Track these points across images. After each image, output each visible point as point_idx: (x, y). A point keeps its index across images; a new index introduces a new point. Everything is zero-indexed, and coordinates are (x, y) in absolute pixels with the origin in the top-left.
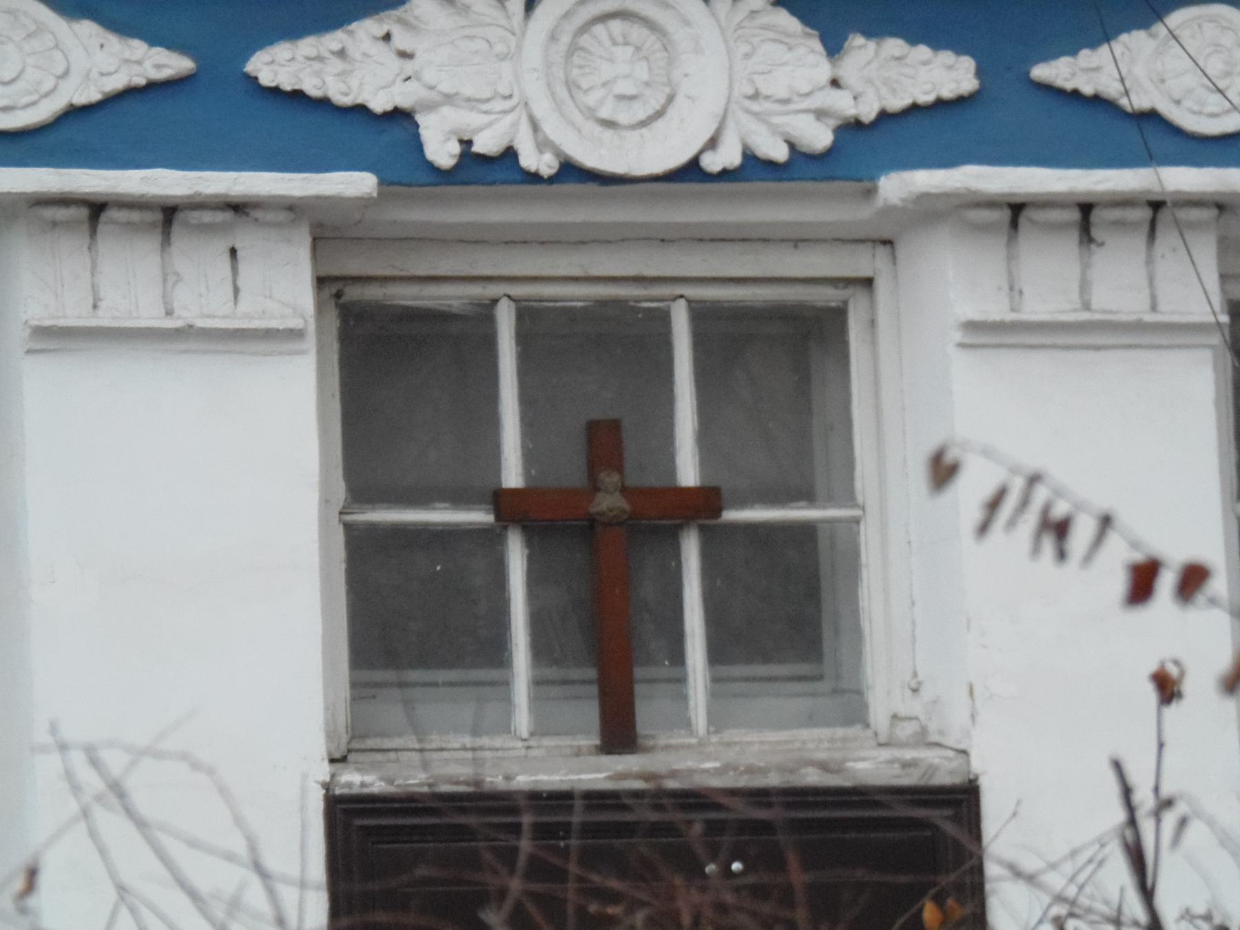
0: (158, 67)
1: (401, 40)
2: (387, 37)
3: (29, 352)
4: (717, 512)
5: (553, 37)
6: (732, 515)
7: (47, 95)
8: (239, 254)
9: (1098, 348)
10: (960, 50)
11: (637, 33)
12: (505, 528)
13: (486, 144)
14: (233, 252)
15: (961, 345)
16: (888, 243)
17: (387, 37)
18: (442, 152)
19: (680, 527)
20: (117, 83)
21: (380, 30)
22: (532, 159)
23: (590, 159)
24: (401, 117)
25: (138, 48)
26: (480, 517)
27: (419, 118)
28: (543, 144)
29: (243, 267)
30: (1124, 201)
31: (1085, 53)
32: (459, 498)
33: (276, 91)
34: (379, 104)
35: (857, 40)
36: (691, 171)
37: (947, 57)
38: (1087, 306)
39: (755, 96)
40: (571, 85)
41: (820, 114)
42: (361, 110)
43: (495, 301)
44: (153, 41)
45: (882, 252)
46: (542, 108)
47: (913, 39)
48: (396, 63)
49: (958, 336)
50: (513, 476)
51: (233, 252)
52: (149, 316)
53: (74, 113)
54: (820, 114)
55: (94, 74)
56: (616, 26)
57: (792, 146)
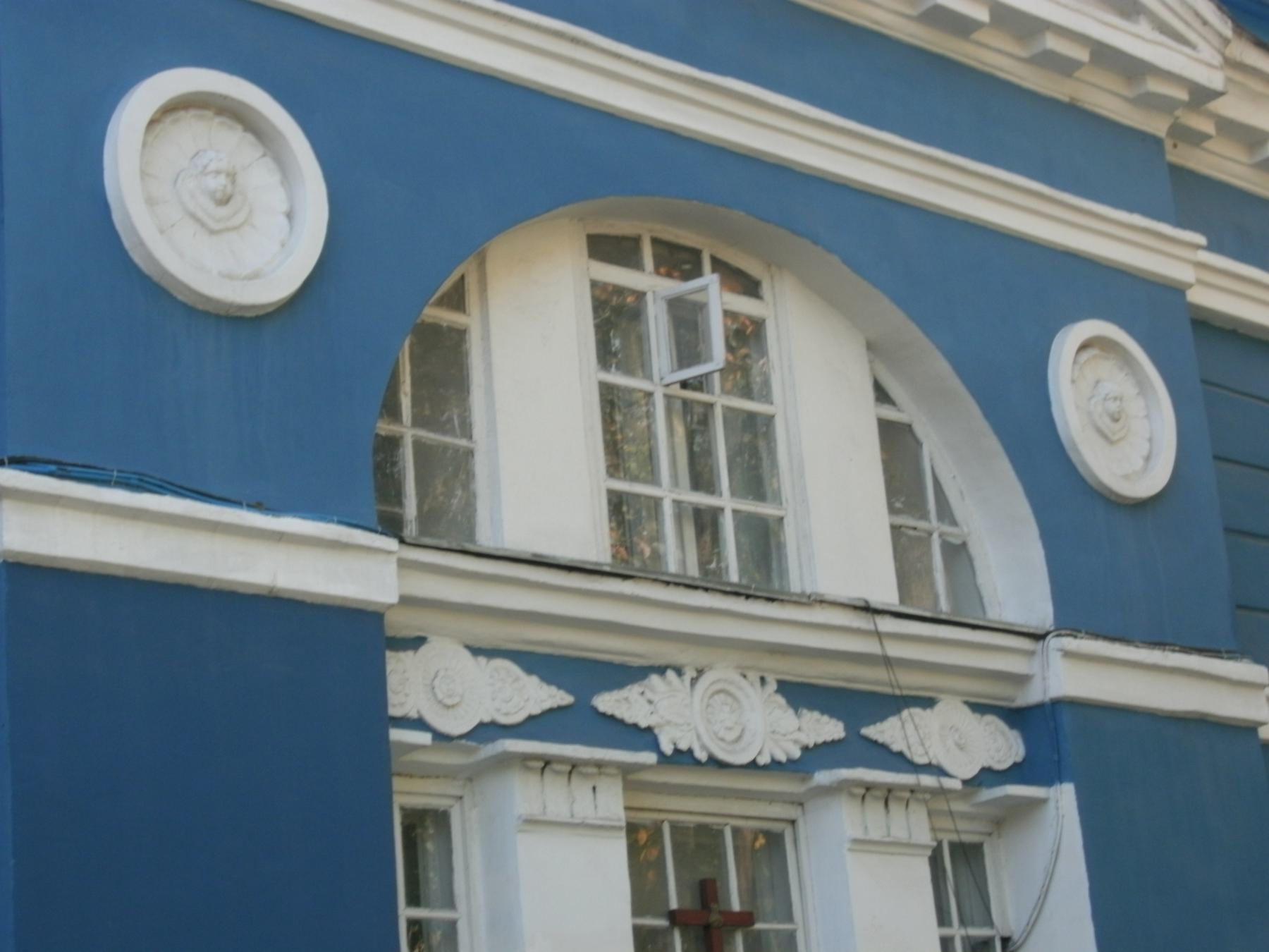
0: (562, 699)
1: (649, 695)
2: (643, 693)
3: (520, 831)
4: (753, 924)
5: (702, 700)
6: (759, 926)
7: (521, 709)
8: (597, 789)
9: (892, 854)
10: (839, 718)
11: (730, 700)
12: (673, 928)
13: (683, 746)
14: (594, 788)
15: (850, 850)
16: (801, 804)
17: (643, 693)
18: (667, 749)
19: (734, 931)
20: (547, 705)
21: (641, 690)
22: (701, 755)
23: (721, 755)
24: (649, 730)
25: (553, 690)
26: (663, 923)
27: (656, 731)
28: (704, 747)
29: (598, 795)
30: (903, 787)
31: (878, 724)
32: (656, 915)
33: (604, 715)
34: (643, 724)
35: (805, 711)
36: (753, 765)
37: (833, 722)
38: (889, 835)
39: (773, 732)
40: (709, 721)
41: (796, 742)
42: (635, 726)
43: (663, 821)
44: (560, 687)
45: (800, 809)
46: (702, 730)
47: (823, 712)
48: (648, 707)
49: (848, 845)
50: (674, 904)
51: (594, 788)
52: (564, 816)
53: (531, 718)
54: (796, 742)
55: (690, 674)
56: (722, 696)
57: (787, 754)
